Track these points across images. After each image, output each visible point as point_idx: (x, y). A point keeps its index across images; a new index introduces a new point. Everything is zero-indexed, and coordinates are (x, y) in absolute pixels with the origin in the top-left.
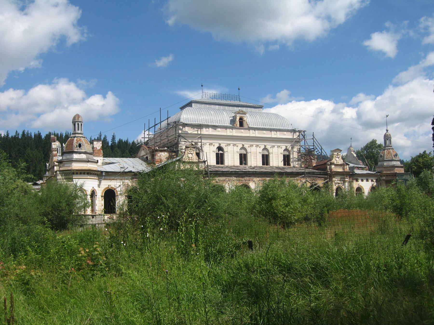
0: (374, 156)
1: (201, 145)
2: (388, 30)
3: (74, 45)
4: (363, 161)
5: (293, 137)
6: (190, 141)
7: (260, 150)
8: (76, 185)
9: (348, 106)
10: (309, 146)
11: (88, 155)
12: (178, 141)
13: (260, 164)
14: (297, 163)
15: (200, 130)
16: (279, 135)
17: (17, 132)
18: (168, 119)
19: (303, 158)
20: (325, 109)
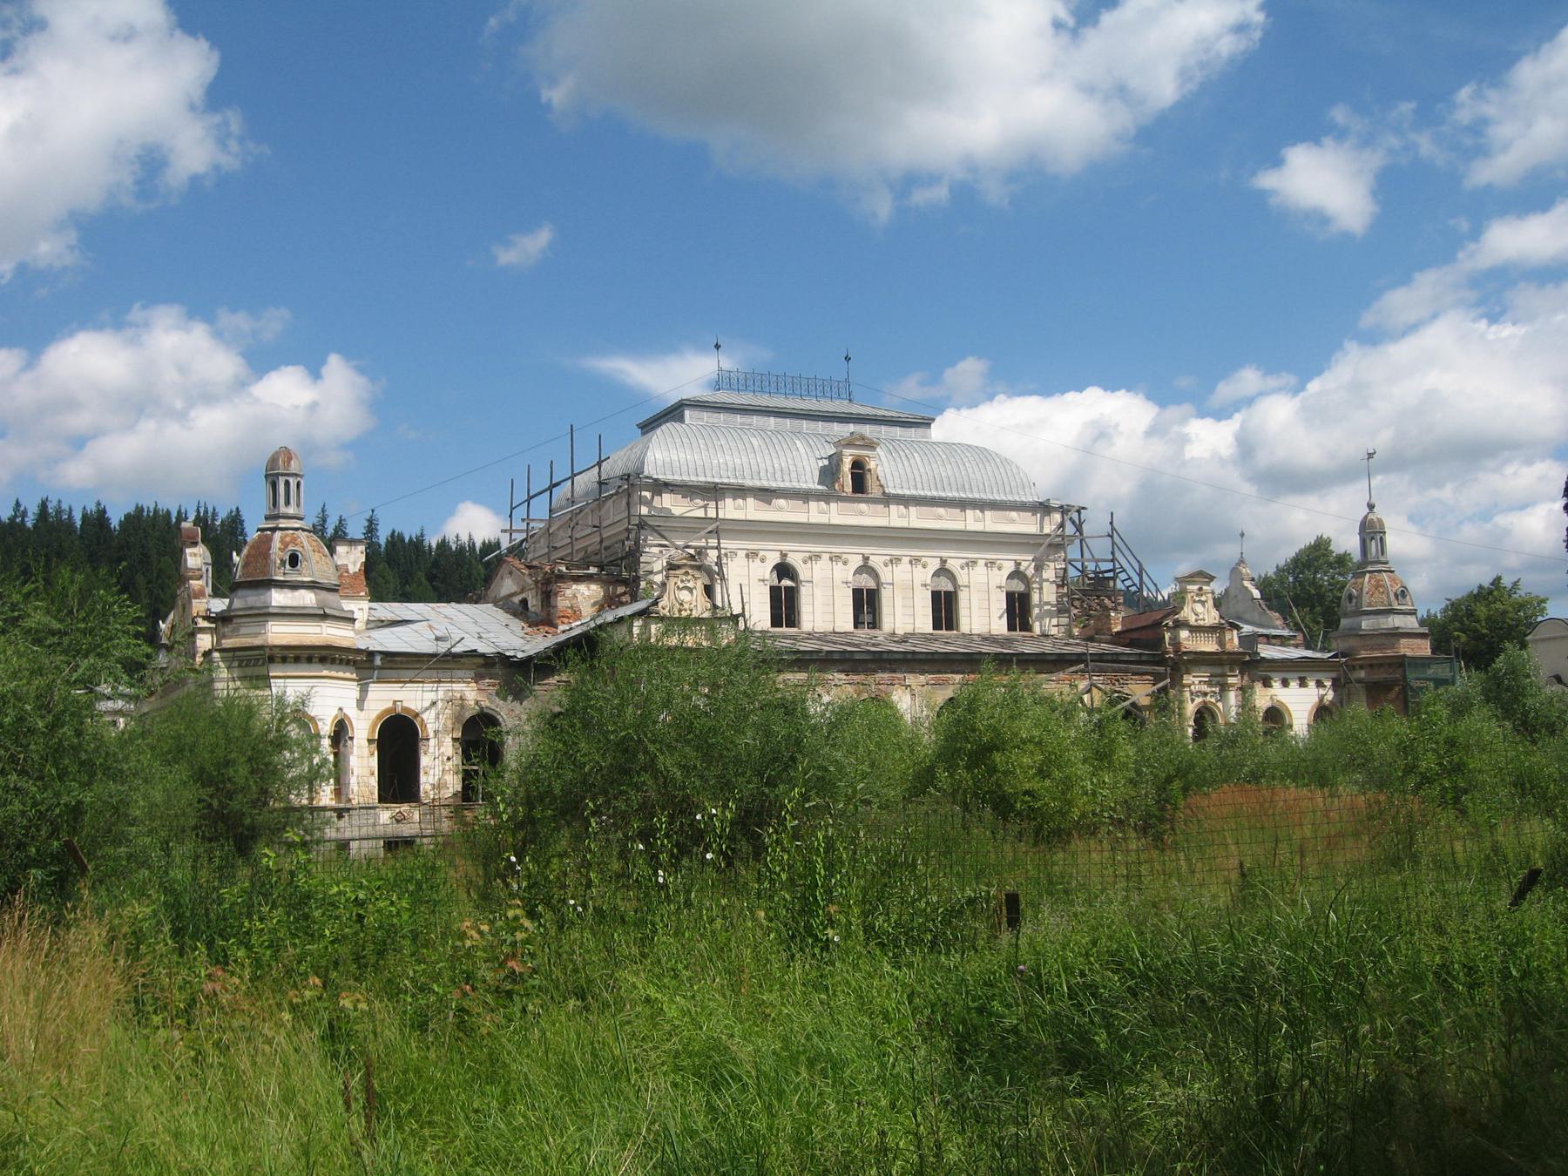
0: (1321, 597)
1: (719, 557)
2: (1340, 134)
3: (195, 180)
4: (1285, 613)
5: (1042, 528)
6: (680, 543)
7: (924, 575)
8: (281, 700)
9: (1202, 415)
10: (1097, 561)
11: (324, 594)
12: (637, 543)
13: (925, 624)
14: (1054, 621)
15: (712, 504)
16: (990, 522)
17: (18, 504)
18: (599, 464)
19: (1077, 603)
20: (1117, 425)
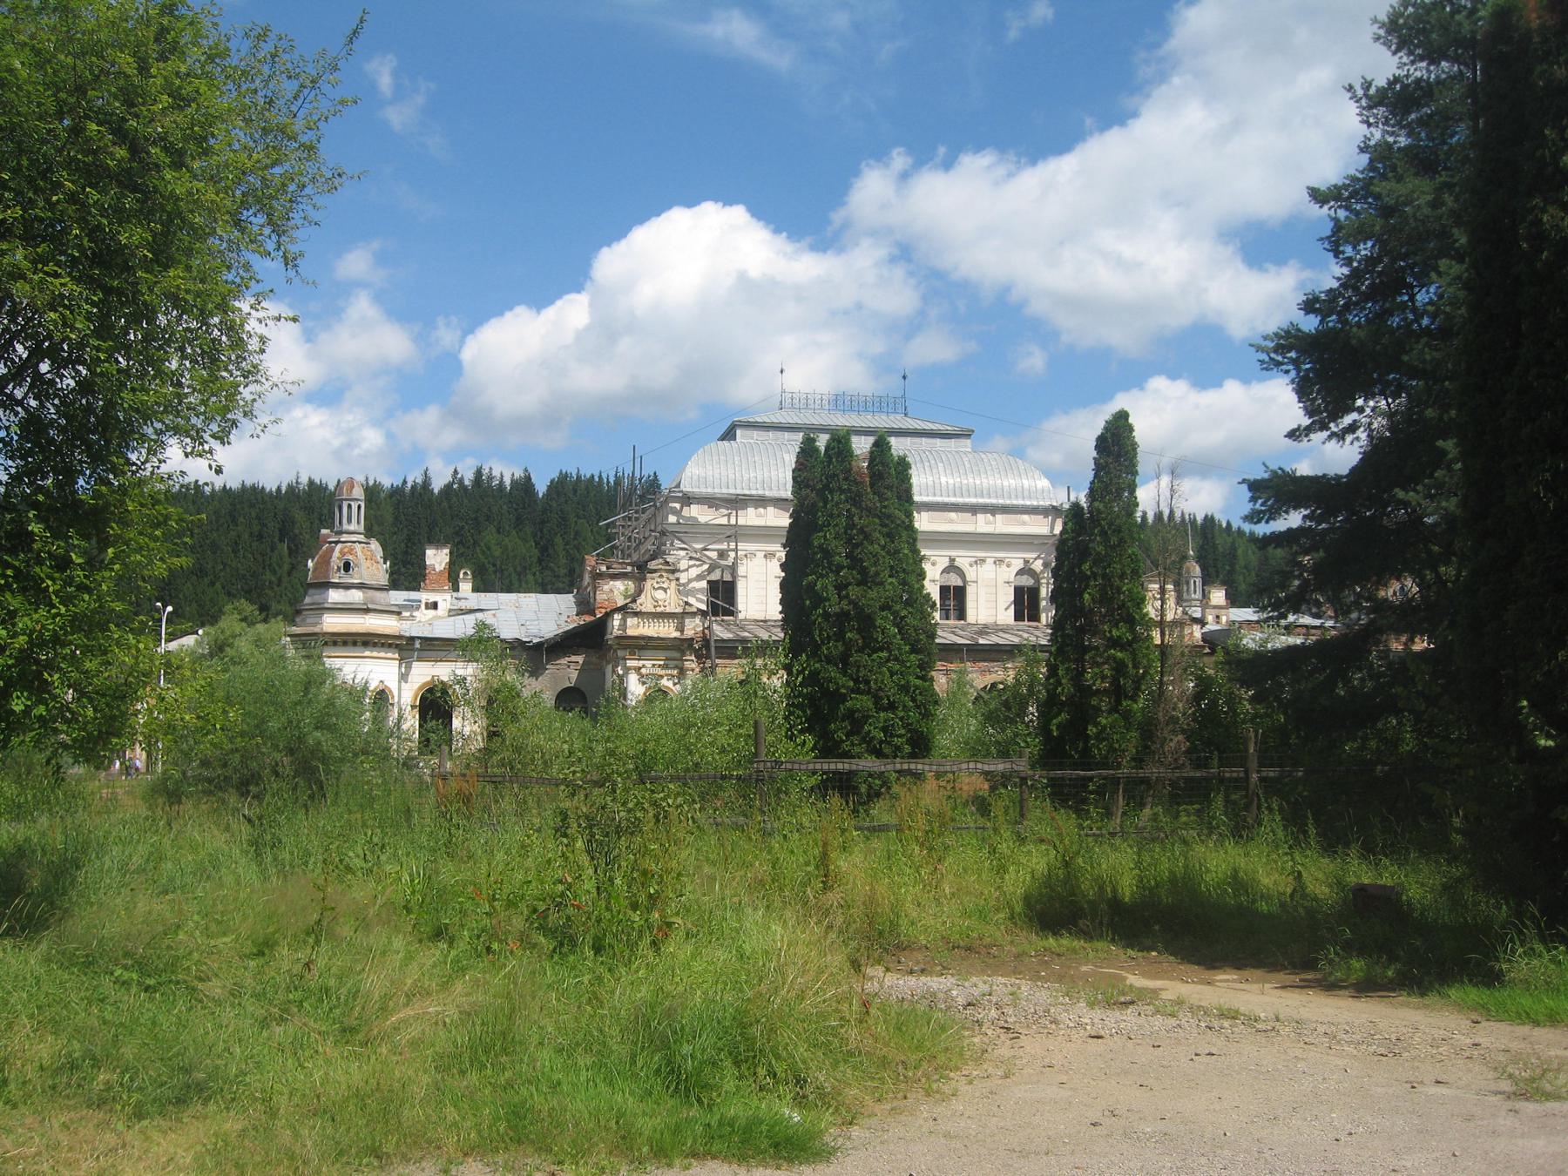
11: (371, 593)
17: (456, 472)
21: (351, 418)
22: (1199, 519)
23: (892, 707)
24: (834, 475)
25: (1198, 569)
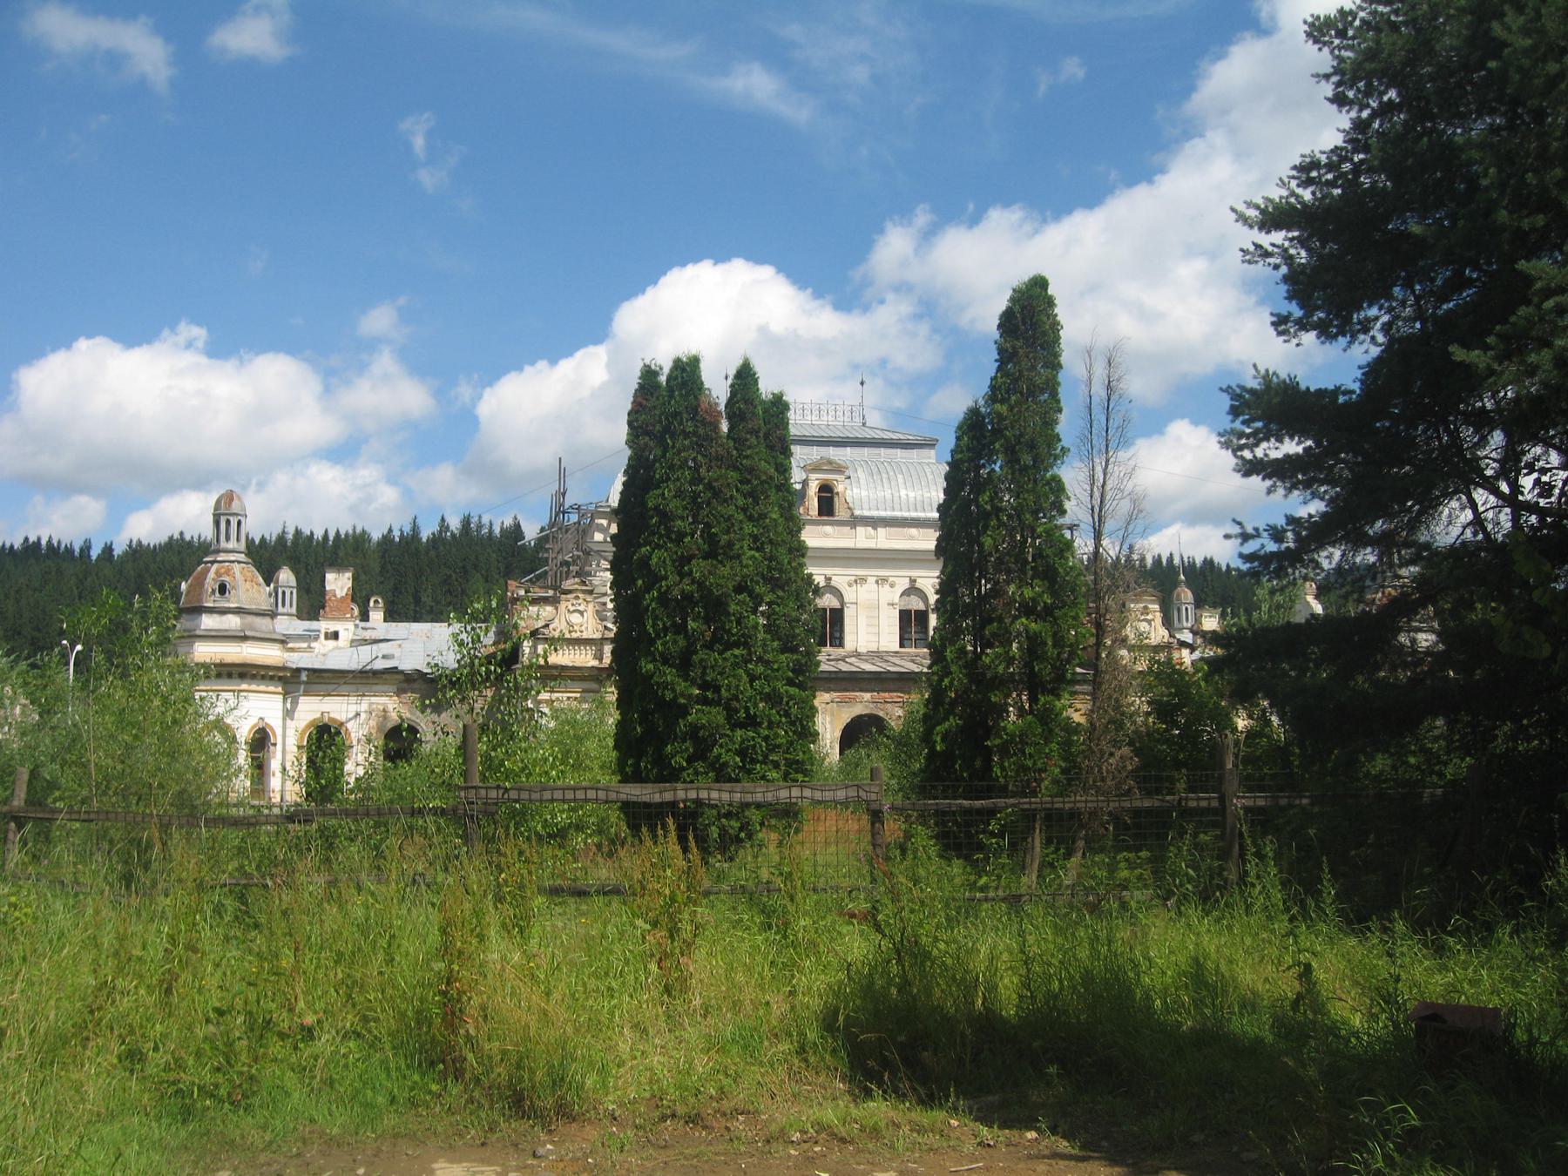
11: (250, 619)
17: (443, 519)
21: (367, 473)
22: (1199, 562)
23: (752, 722)
24: (676, 414)
25: (1190, 594)
